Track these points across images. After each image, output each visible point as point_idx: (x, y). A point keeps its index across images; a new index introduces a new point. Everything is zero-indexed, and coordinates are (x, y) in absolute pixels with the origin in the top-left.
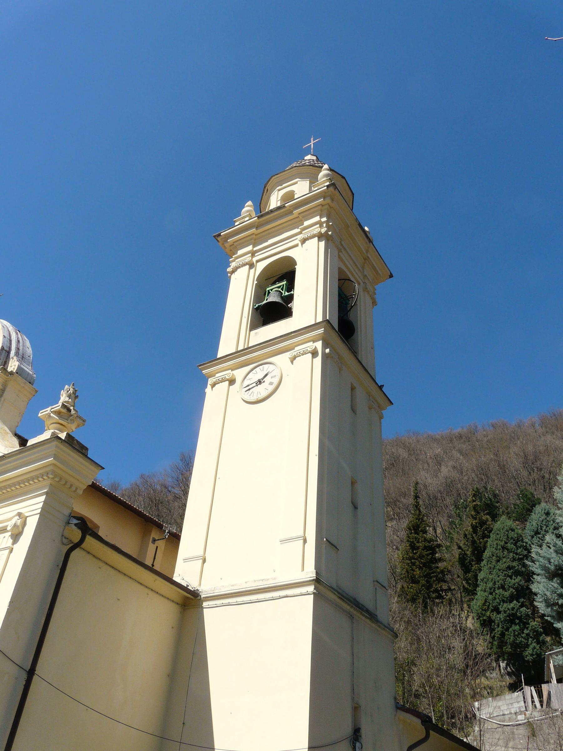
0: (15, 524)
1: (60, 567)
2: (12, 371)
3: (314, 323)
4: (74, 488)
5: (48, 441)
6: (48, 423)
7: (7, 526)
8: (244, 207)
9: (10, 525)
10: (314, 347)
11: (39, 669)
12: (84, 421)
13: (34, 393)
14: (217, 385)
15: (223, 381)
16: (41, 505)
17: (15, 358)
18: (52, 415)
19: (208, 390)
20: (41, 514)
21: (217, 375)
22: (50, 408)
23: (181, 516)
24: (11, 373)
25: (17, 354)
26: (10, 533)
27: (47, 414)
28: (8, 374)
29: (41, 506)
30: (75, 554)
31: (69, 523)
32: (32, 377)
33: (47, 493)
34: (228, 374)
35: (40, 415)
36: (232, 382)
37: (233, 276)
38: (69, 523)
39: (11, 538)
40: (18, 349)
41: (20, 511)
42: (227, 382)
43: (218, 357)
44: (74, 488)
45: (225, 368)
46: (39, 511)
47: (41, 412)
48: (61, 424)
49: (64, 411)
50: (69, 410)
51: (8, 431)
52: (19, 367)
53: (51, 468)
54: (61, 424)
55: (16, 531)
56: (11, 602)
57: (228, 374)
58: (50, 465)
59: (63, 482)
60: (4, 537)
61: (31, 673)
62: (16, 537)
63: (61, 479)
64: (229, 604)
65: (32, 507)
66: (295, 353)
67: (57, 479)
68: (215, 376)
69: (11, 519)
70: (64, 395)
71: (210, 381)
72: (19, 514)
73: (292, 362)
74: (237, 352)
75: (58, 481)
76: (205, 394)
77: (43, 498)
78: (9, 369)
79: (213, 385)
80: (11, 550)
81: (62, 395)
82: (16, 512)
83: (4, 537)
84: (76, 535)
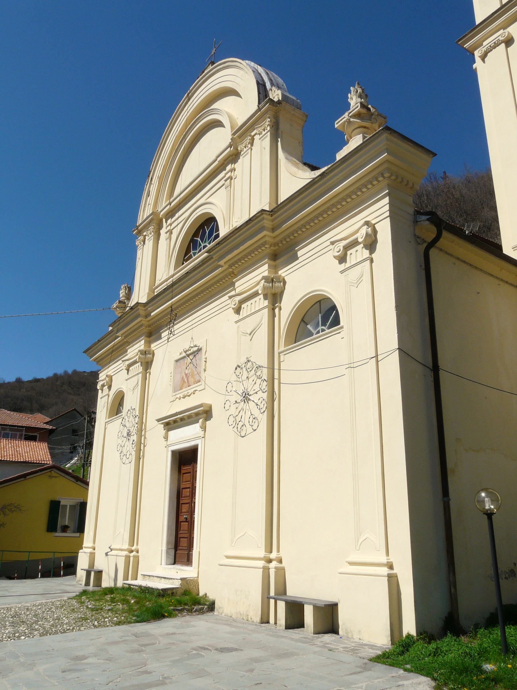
0: (367, 233)
1: (423, 267)
2: (279, 100)
3: (499, 6)
4: (410, 185)
5: (362, 146)
6: (347, 131)
7: (357, 238)
8: (243, 60)
9: (259, 288)
10: (507, 34)
11: (441, 363)
12: (385, 118)
13: (304, 119)
14: (489, 54)
15: (496, 45)
16: (387, 207)
17: (274, 88)
18: (352, 120)
19: (478, 65)
20: (391, 216)
21: (485, 43)
22: (347, 114)
23: (147, 363)
24: (279, 102)
25: (272, 84)
26: (362, 245)
27: (345, 122)
28: (275, 104)
29: (388, 209)
30: (433, 253)
31: (417, 222)
32: (298, 103)
33: (388, 194)
34: (501, 35)
35: (336, 126)
36: (509, 42)
37: (227, 143)
38: (417, 222)
39: (366, 249)
40: (271, 80)
41: (367, 219)
42: (503, 45)
43: (477, 24)
44: (410, 185)
45: (493, 31)
46: (388, 214)
47: (336, 122)
48: (365, 127)
49: (364, 111)
50: (369, 109)
51: (297, 162)
52: (283, 95)
53: (386, 165)
54: (365, 127)
55: (370, 241)
56: (397, 307)
57: (501, 35)
58: (384, 162)
59: (399, 180)
60: (357, 251)
61: (435, 369)
62: (371, 244)
63: (397, 177)
64: (147, 406)
65: (378, 213)
66: (485, 49)
67: (393, 178)
68: (482, 45)
69: (258, 284)
70: (354, 98)
71: (477, 54)
72: (367, 223)
73: (484, 62)
74: (502, 6)
75: (394, 180)
76: (474, 73)
77: (387, 200)
78: (276, 99)
79: (483, 58)
80: (372, 261)
81: (352, 99)
82: (363, 222)
83: (357, 251)
84: (429, 232)
